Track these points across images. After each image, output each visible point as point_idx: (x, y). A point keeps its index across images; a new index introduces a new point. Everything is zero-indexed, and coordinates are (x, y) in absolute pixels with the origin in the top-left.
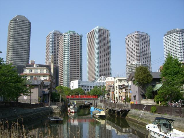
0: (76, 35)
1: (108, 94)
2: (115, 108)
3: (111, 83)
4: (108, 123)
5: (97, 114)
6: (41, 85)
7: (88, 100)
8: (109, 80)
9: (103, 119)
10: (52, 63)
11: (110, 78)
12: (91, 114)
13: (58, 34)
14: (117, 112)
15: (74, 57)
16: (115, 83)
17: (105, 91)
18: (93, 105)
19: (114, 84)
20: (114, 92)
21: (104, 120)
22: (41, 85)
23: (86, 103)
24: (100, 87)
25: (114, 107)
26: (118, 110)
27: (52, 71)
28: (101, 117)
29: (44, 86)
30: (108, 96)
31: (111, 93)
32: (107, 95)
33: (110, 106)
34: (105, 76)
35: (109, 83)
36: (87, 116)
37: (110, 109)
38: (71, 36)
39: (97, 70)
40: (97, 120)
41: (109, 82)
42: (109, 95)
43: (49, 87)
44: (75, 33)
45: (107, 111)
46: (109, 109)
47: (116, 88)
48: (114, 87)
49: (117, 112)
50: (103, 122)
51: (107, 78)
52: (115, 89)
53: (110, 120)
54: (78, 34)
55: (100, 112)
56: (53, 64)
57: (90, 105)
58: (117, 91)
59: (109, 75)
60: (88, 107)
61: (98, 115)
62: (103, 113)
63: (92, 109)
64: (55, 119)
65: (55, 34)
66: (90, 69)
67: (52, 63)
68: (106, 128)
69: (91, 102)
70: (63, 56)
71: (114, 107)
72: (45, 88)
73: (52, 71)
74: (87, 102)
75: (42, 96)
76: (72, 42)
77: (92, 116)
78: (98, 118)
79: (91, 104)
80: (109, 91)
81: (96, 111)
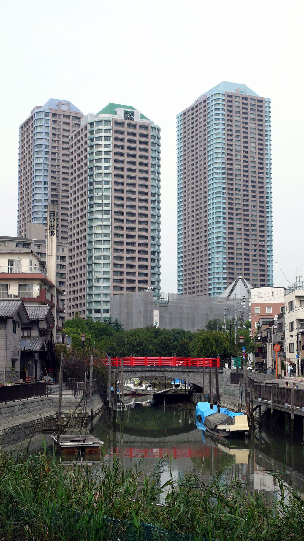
0: (137, 119)
1: (261, 352)
2: (287, 405)
3: (269, 311)
4: (260, 462)
5: (220, 427)
6: (16, 318)
7: (186, 374)
8: (260, 296)
9: (241, 446)
10: (52, 234)
11: (265, 290)
12: (201, 427)
13: (64, 116)
14: (293, 417)
15: (129, 162)
16: (286, 310)
17: (248, 340)
18: (206, 390)
19: (281, 316)
20: (281, 343)
21: (246, 447)
22: (16, 318)
23: (177, 386)
24: (231, 325)
25: (283, 400)
26: (295, 412)
27: (52, 263)
28: (237, 439)
29: (26, 321)
30: (260, 360)
31: (269, 348)
32: (257, 355)
33: (267, 396)
34: (248, 280)
35: (263, 310)
36: (183, 437)
37: (268, 410)
38: (117, 123)
39: (219, 256)
40: (220, 446)
41: (263, 306)
42: (264, 355)
43: (43, 325)
44: (133, 113)
45: (256, 415)
46: (263, 409)
47: (292, 330)
48: (281, 325)
49: (293, 417)
50: (241, 456)
51: (255, 292)
52: (288, 334)
53: (266, 450)
54: (143, 117)
55: (231, 421)
56: (54, 238)
57: (191, 392)
58: (294, 340)
59: (263, 280)
60: (186, 399)
61: (224, 431)
62: (241, 423)
63: (203, 408)
64: (72, 441)
65: (54, 115)
66: (191, 262)
67: (52, 234)
68: (250, 483)
69: (198, 379)
70: (84, 205)
71: (283, 400)
72: (30, 329)
73: (52, 263)
74: (181, 382)
75: (19, 358)
76: (122, 176)
77: (205, 435)
78: (226, 441)
79: (198, 389)
80: (264, 340)
81: (219, 416)
